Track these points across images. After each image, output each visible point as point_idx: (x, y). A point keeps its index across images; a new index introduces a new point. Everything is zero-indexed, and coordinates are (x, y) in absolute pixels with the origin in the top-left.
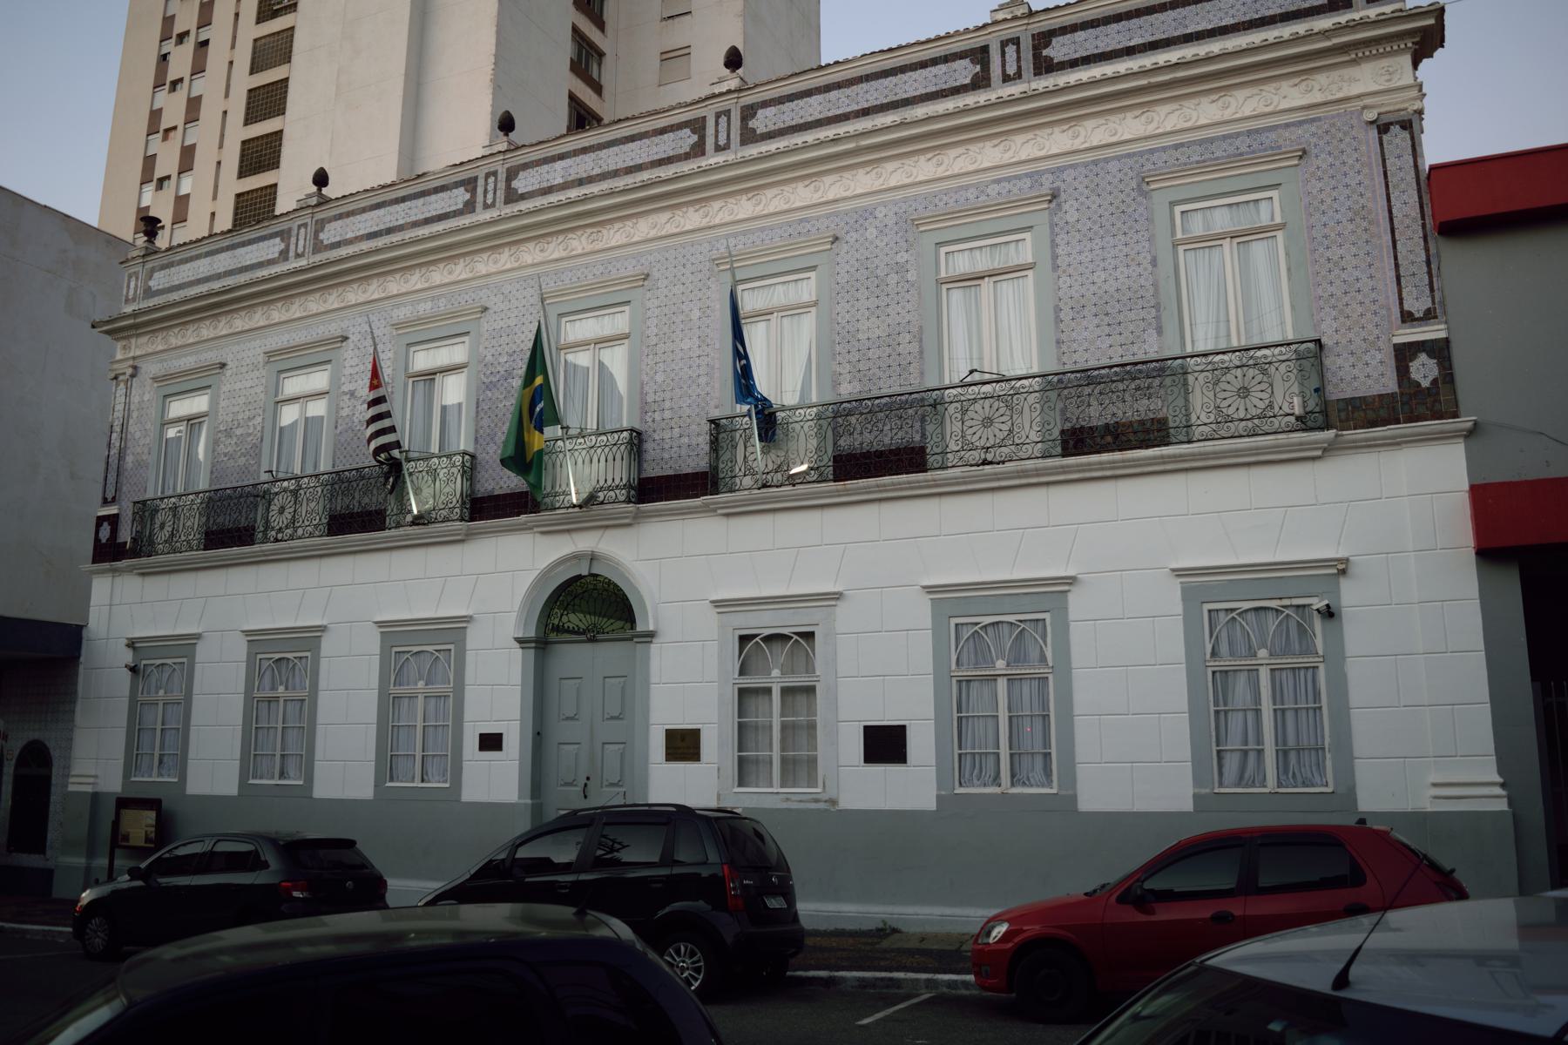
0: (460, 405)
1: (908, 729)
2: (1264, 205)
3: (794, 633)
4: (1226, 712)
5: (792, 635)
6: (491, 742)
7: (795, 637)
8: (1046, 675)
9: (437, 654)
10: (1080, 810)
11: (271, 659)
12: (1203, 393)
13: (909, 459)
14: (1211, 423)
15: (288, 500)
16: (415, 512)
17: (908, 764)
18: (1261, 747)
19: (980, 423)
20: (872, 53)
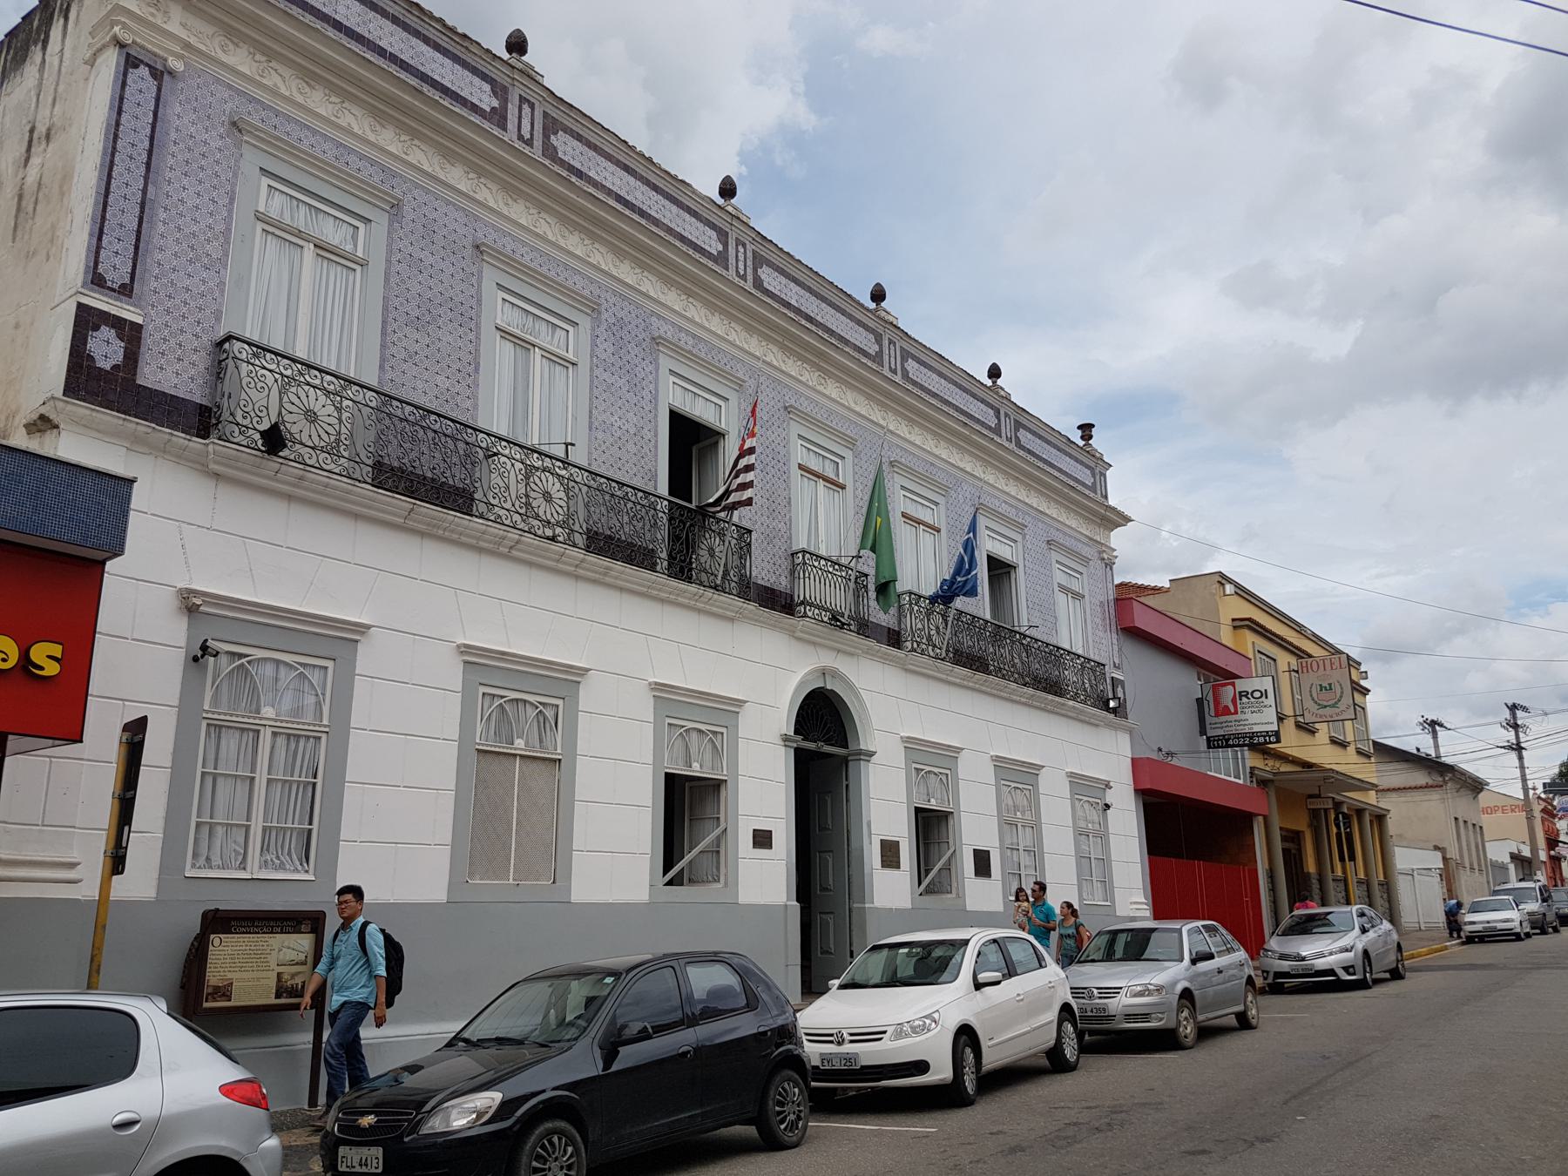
0: (905, 747)
2: (560, 333)
4: (215, 777)
6: (762, 839)
8: (319, 735)
9: (541, 708)
11: (683, 727)
13: (459, 499)
15: (544, 481)
17: (992, 878)
18: (249, 823)
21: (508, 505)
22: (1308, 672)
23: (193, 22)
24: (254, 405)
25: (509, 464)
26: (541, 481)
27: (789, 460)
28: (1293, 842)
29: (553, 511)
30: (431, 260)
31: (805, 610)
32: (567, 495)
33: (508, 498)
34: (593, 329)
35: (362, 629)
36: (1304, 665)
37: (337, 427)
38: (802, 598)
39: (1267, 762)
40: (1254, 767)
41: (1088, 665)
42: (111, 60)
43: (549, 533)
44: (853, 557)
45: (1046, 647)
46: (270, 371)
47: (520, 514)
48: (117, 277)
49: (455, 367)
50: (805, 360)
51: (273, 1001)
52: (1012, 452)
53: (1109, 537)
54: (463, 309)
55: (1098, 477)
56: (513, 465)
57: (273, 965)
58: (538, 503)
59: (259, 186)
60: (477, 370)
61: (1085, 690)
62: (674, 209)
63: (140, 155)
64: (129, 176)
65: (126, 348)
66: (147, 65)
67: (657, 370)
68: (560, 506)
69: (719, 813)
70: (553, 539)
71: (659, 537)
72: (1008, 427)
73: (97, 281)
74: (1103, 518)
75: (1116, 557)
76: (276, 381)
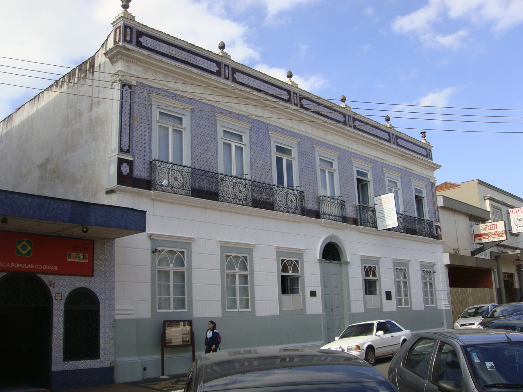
1: (392, 292)
3: (178, 251)
5: (177, 252)
6: (313, 294)
7: (178, 253)
10: (194, 317)
12: (159, 174)
14: (160, 185)
16: (163, 184)
19: (178, 179)
20: (245, 66)
21: (229, 196)
22: (513, 214)
23: (138, 68)
24: (162, 178)
25: (228, 183)
26: (175, 173)
27: (315, 164)
28: (510, 277)
29: (242, 195)
30: (203, 123)
31: (324, 216)
32: (246, 190)
33: (229, 194)
34: (250, 133)
35: (193, 239)
36: (512, 211)
37: (182, 181)
38: (322, 212)
39: (498, 249)
40: (492, 252)
41: (426, 222)
42: (119, 86)
43: (241, 203)
44: (339, 197)
45: (402, 216)
46: (165, 168)
47: (233, 198)
48: (125, 148)
49: (211, 155)
50: (318, 128)
51: (181, 343)
52: (396, 149)
53: (433, 174)
54: (212, 136)
55: (428, 152)
56: (229, 183)
57: (181, 334)
58: (237, 193)
59: (157, 111)
60: (217, 154)
61: (425, 231)
62: (273, 87)
63: (128, 111)
64: (126, 119)
65: (129, 168)
66: (127, 85)
67: (270, 142)
68: (180, 183)
69: (298, 286)
70: (243, 205)
71: (274, 199)
72: (393, 139)
73: (121, 150)
74: (431, 167)
75: (436, 181)
76: (167, 170)
